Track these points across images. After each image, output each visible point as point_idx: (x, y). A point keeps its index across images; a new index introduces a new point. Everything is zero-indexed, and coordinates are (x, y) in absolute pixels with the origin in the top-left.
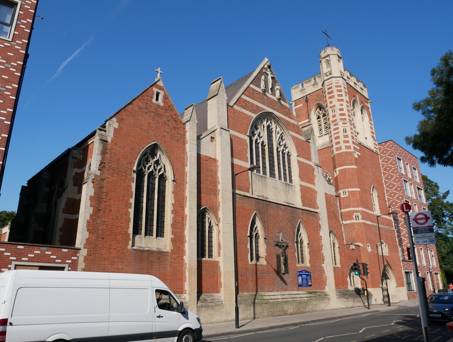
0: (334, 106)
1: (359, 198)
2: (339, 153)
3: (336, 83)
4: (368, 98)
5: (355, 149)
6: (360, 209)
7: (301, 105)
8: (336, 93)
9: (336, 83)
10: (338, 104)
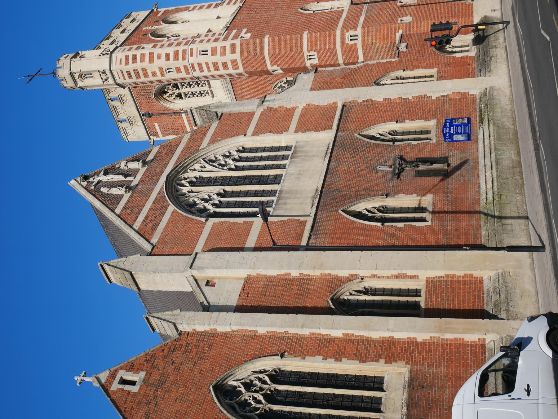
0: (161, 69)
1: (320, 34)
2: (243, 64)
3: (121, 64)
4: (147, 12)
5: (235, 37)
6: (338, 33)
7: (156, 125)
8: (139, 65)
9: (121, 64)
10: (158, 63)
